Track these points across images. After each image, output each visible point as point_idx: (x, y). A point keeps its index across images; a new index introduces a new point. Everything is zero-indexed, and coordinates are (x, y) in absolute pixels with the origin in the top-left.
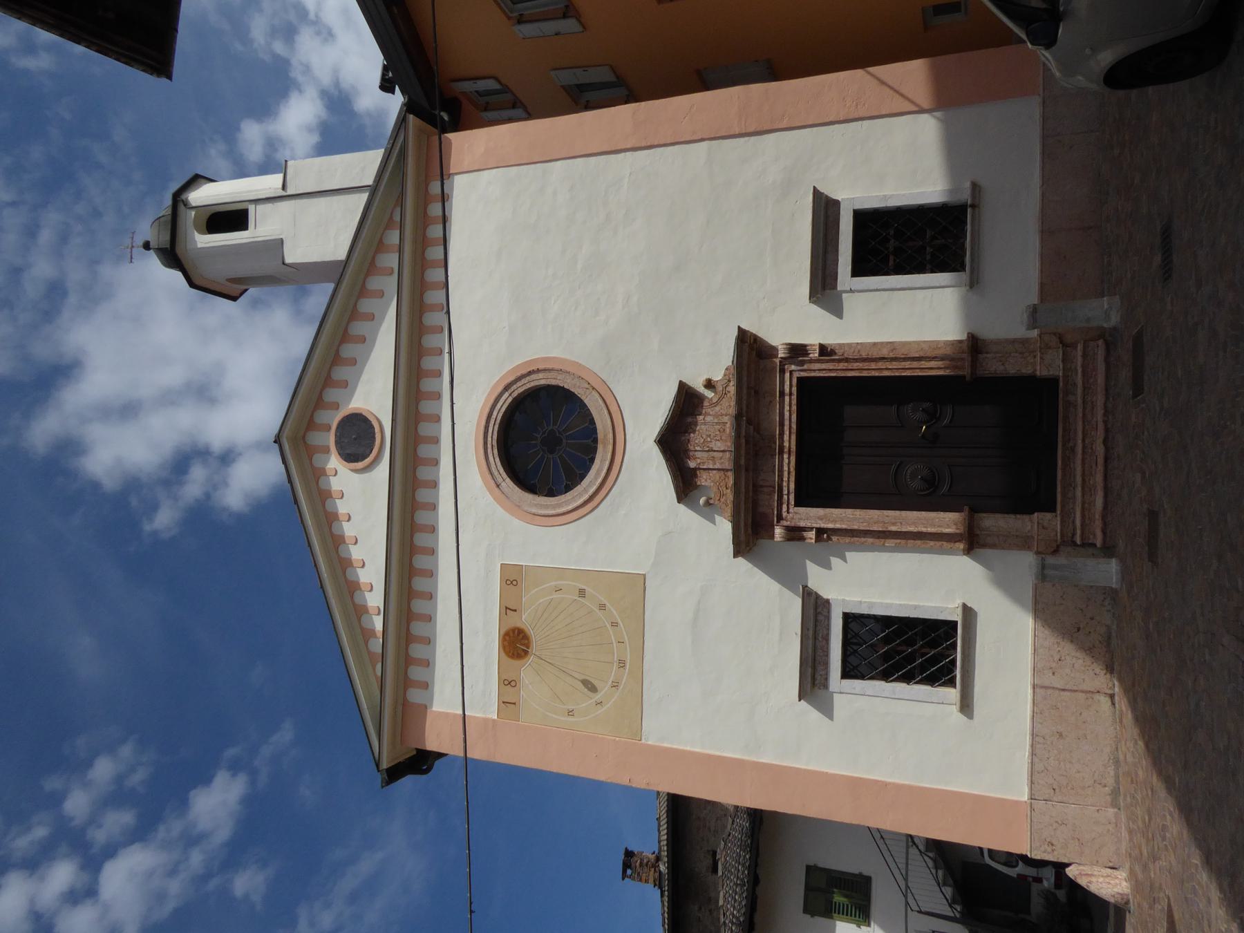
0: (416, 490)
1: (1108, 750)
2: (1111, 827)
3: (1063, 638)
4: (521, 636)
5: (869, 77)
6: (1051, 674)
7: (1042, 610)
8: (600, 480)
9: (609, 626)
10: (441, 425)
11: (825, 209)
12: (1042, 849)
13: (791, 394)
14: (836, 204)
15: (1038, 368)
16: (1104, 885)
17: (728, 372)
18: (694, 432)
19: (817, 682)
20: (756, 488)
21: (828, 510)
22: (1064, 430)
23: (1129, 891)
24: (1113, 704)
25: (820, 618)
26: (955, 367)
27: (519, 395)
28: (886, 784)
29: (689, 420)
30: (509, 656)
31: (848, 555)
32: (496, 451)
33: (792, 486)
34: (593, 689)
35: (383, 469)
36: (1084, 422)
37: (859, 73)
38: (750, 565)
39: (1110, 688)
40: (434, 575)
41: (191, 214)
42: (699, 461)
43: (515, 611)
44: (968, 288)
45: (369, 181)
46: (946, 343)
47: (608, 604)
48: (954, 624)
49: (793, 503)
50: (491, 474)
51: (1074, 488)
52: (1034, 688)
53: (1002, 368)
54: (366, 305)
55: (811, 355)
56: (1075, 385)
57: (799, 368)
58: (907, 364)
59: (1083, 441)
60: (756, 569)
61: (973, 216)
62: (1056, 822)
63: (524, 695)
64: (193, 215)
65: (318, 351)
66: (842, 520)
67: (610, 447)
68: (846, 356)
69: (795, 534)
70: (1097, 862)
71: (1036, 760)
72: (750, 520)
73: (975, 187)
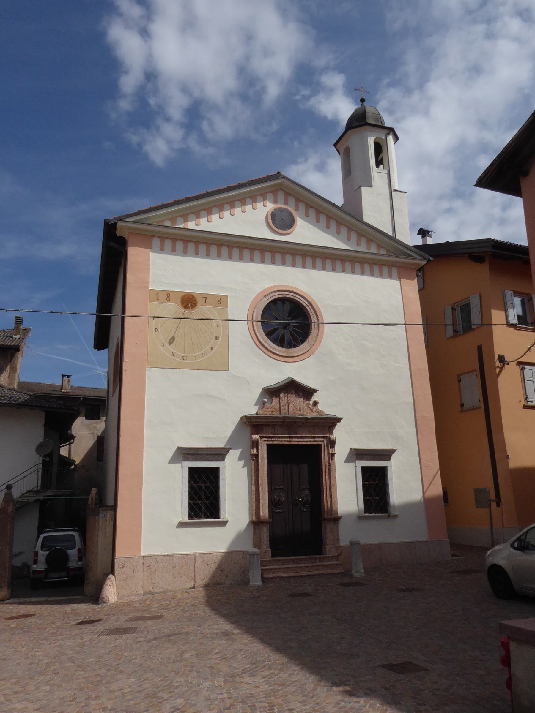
0: (260, 251)
1: (169, 588)
2: (135, 592)
3: (217, 565)
4: (193, 305)
5: (437, 471)
6: (201, 561)
7: (229, 555)
8: (271, 349)
9: (202, 352)
10: (291, 267)
11: (386, 455)
12: (120, 563)
13: (314, 441)
14: (389, 459)
15: (329, 546)
16: (110, 592)
17: (321, 412)
18: (296, 396)
19: (186, 455)
20: (273, 426)
21: (266, 459)
22: (305, 559)
23: (111, 603)
24: (190, 589)
25: (217, 457)
26: (328, 512)
27: (307, 310)
28: (141, 490)
29: (301, 394)
30: (182, 297)
31: (246, 468)
32: (281, 296)
33: (275, 443)
34: (171, 341)
35: (269, 235)
36: (312, 566)
37: (438, 467)
38: (237, 423)
39: (197, 587)
40: (218, 258)
41: (383, 136)
42: (283, 398)
43: (205, 302)
44: (358, 515)
45: (398, 237)
46: (337, 508)
47: (213, 352)
48: (218, 517)
49: (268, 443)
50: (270, 293)
51: (282, 564)
52: (194, 554)
53: (328, 531)
54: (354, 236)
55: (330, 450)
56: (323, 561)
57: (325, 445)
58: (328, 492)
59: (305, 567)
60: (235, 425)
61: (385, 516)
62: (134, 568)
63: (163, 305)
64: (382, 137)
65: (311, 196)
66: (262, 466)
67: (286, 355)
68: (331, 465)
69: (255, 445)
70: (118, 588)
71: (162, 557)
72: (260, 423)
73: (395, 516)
